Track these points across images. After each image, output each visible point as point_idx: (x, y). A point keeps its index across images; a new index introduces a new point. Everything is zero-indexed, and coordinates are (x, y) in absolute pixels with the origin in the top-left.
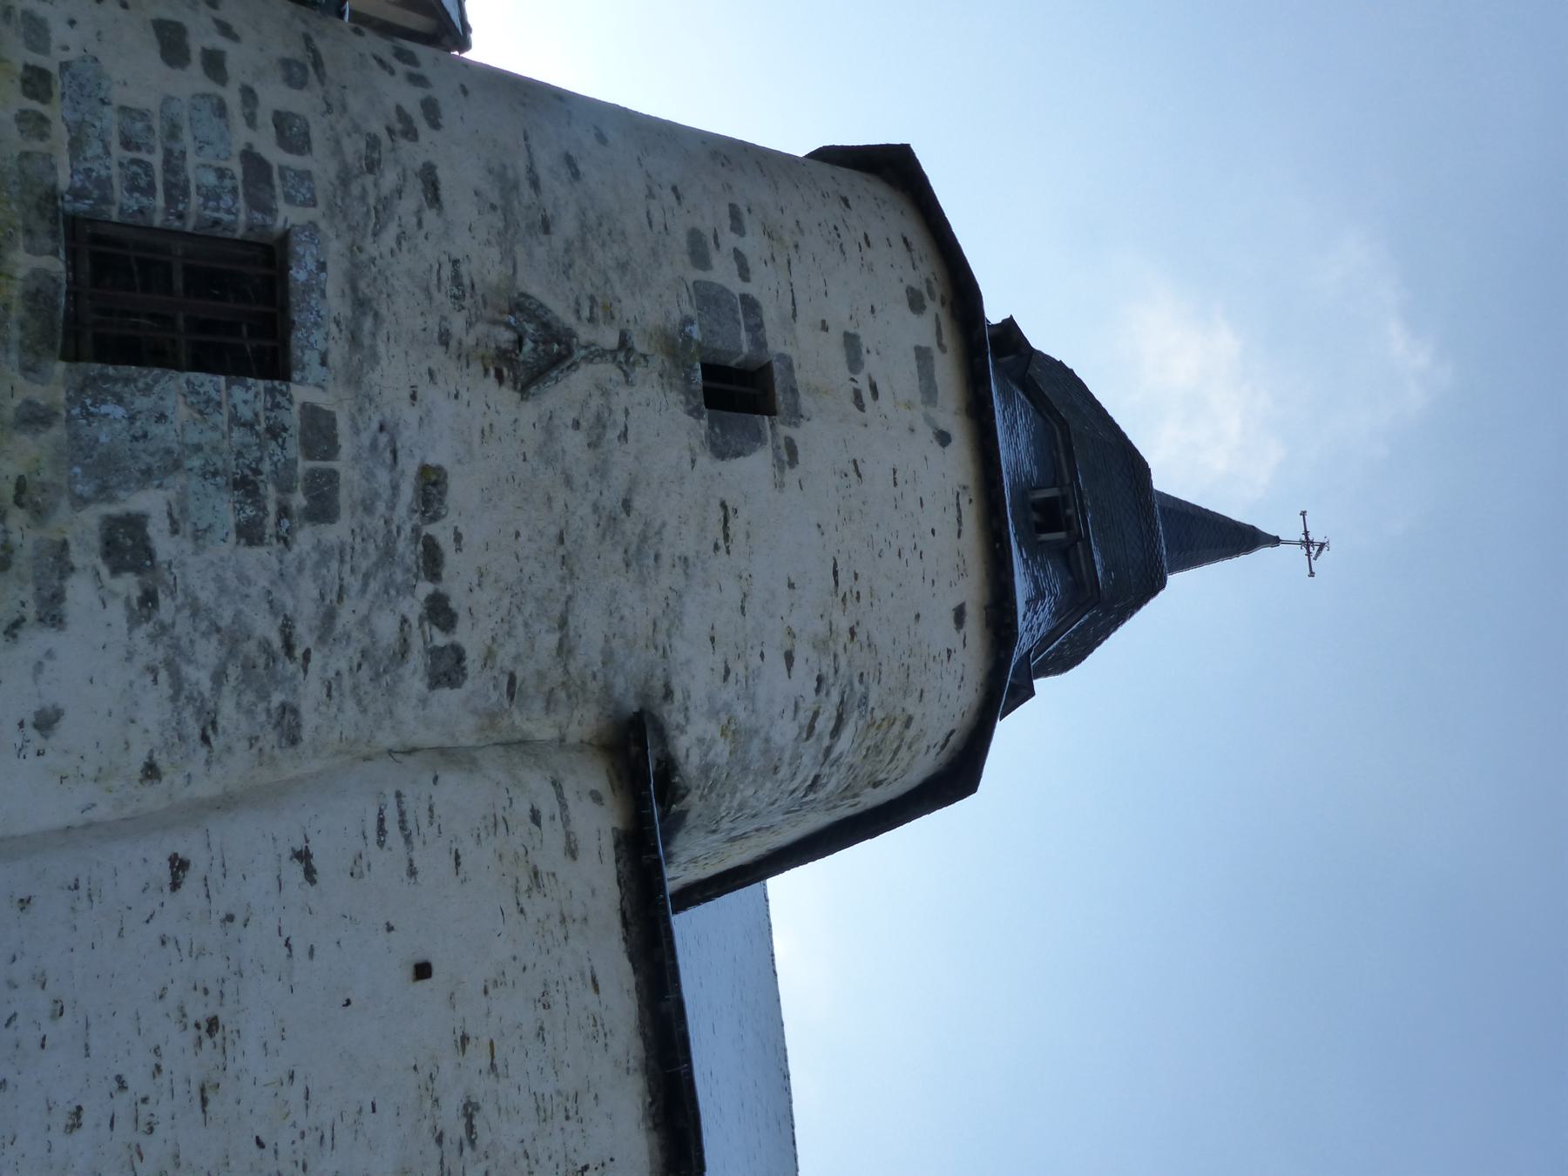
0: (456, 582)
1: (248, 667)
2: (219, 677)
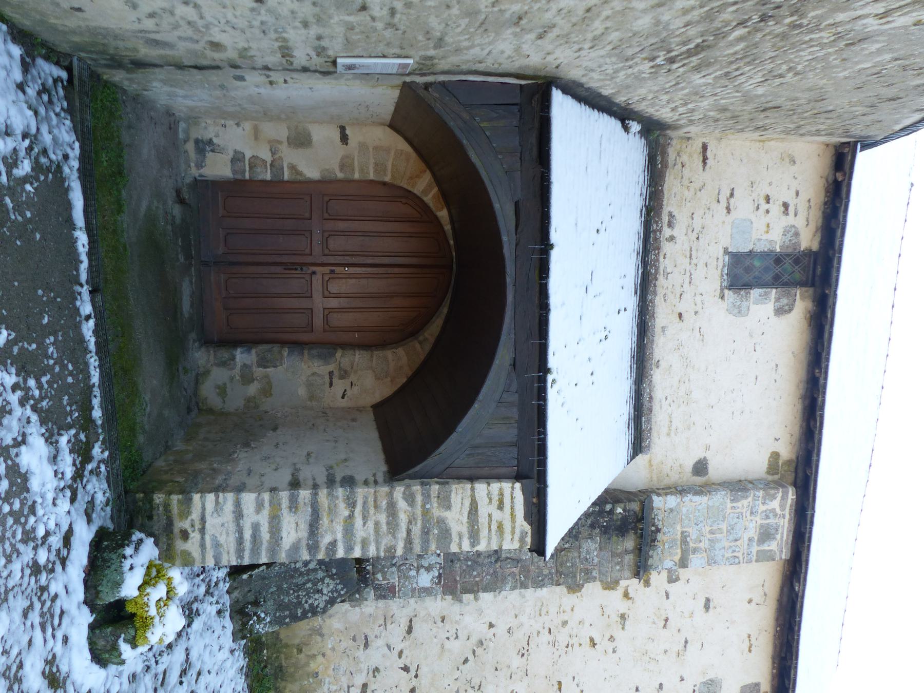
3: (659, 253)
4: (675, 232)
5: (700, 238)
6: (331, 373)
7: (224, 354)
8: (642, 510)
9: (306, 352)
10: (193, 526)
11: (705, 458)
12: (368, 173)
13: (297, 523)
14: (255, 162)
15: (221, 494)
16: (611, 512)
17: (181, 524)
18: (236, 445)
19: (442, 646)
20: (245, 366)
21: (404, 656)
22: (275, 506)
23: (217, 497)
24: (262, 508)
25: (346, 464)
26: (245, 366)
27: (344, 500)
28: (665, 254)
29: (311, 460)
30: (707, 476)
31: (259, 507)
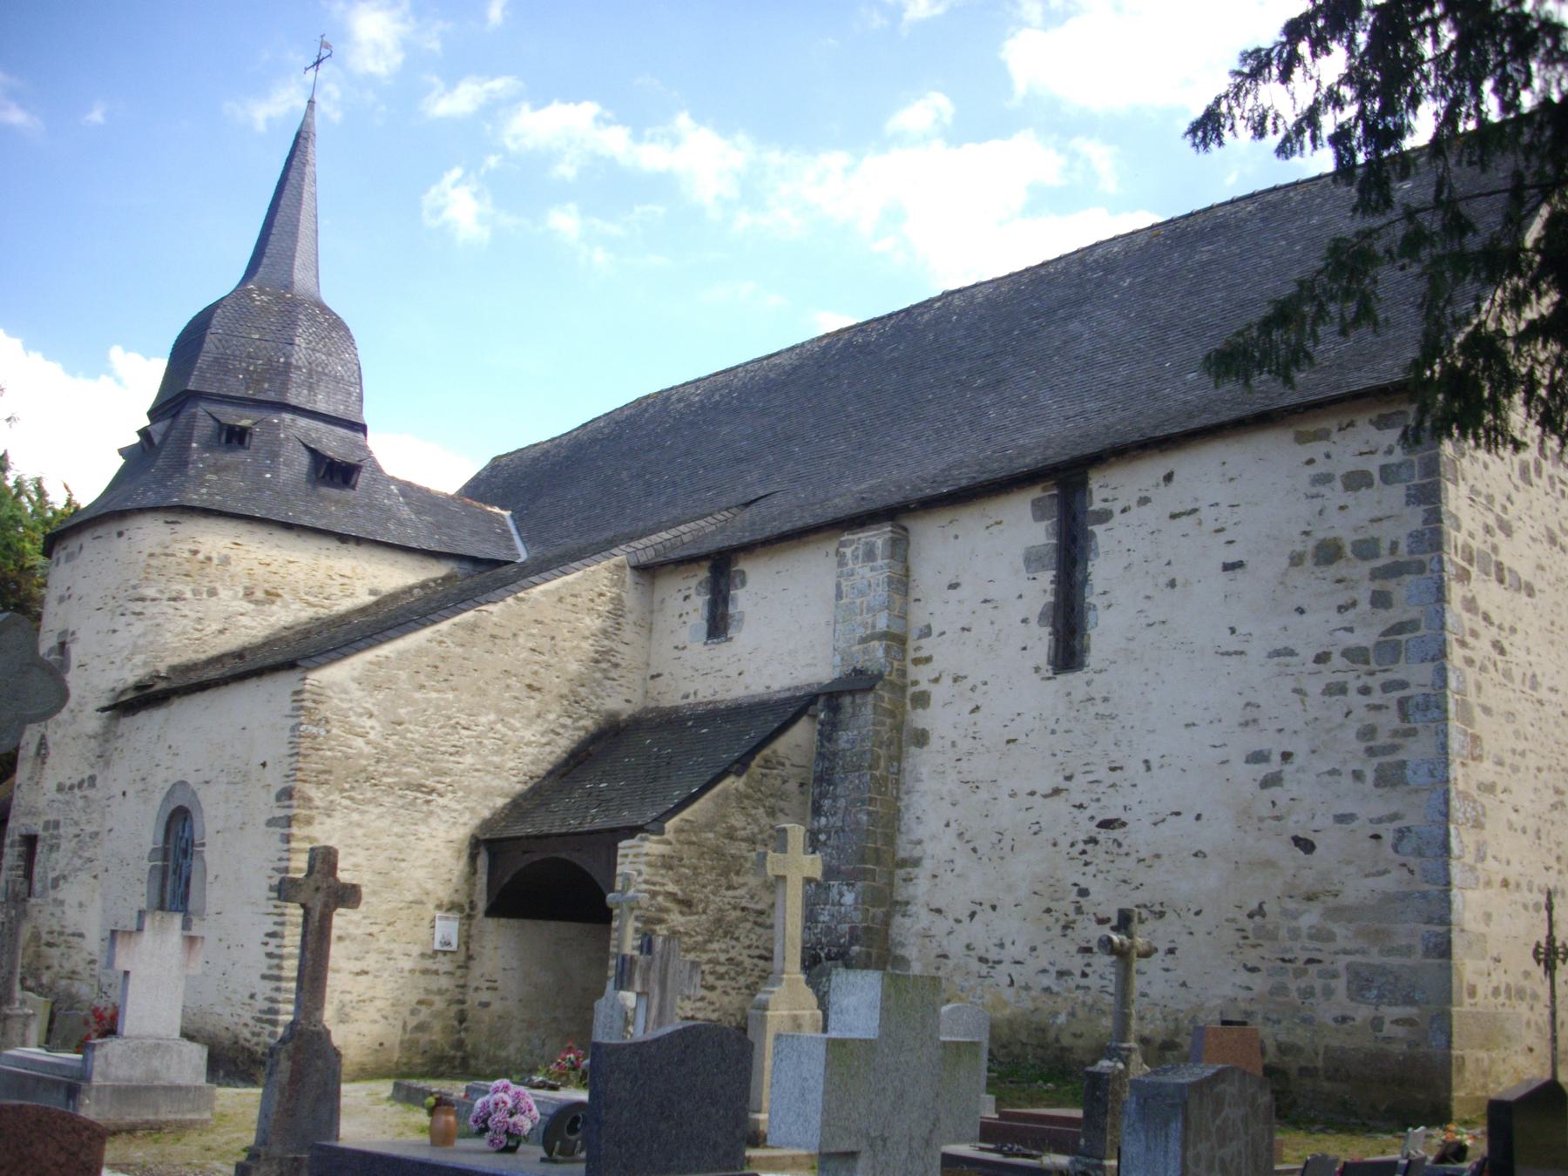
0: (75, 781)
1: (81, 848)
2: (80, 857)
19: (959, 876)
21: (960, 918)
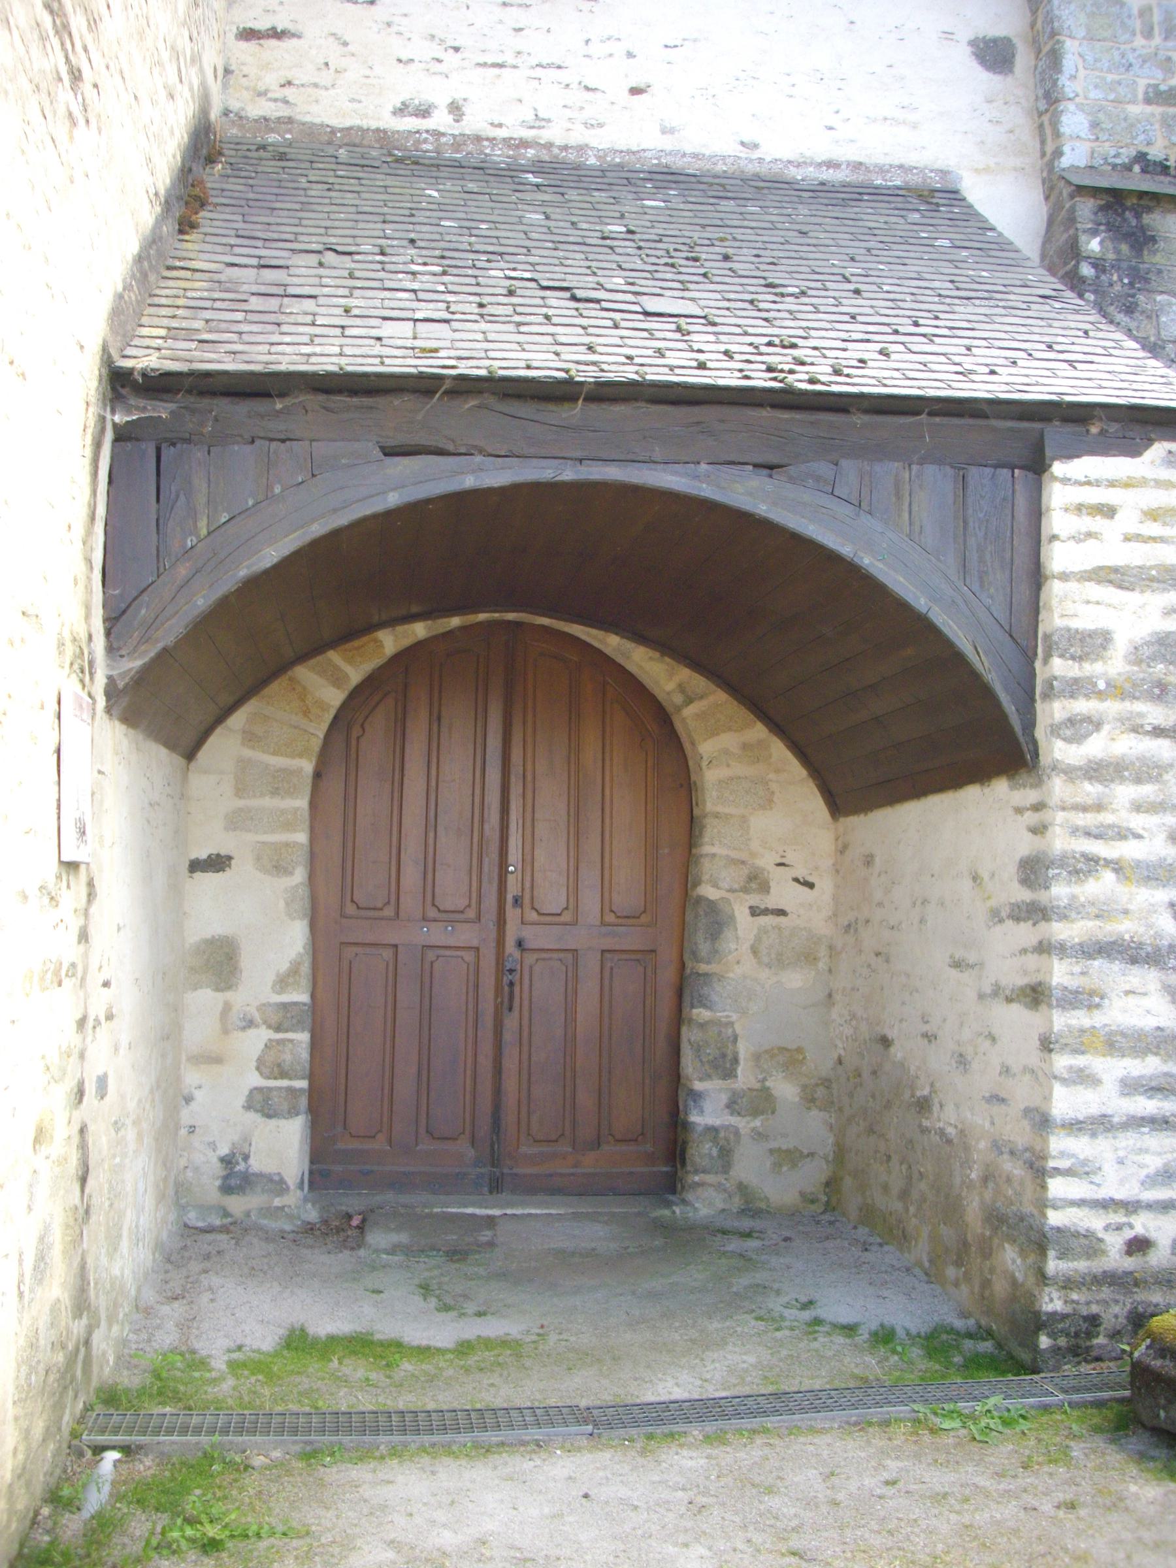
3: (487, 139)
4: (441, 101)
5: (456, 44)
6: (755, 912)
7: (702, 1151)
8: (1095, 191)
9: (703, 968)
10: (1119, 1228)
11: (973, 43)
12: (296, 810)
13: (1128, 993)
14: (271, 1066)
15: (1051, 1164)
16: (1098, 264)
17: (1114, 1257)
18: (924, 1131)
20: (732, 1106)
22: (1081, 1042)
23: (1057, 1171)
24: (1087, 1072)
25: (986, 876)
26: (732, 1106)
27: (1080, 881)
28: (492, 124)
29: (972, 958)
30: (1015, 41)
31: (1084, 1078)
